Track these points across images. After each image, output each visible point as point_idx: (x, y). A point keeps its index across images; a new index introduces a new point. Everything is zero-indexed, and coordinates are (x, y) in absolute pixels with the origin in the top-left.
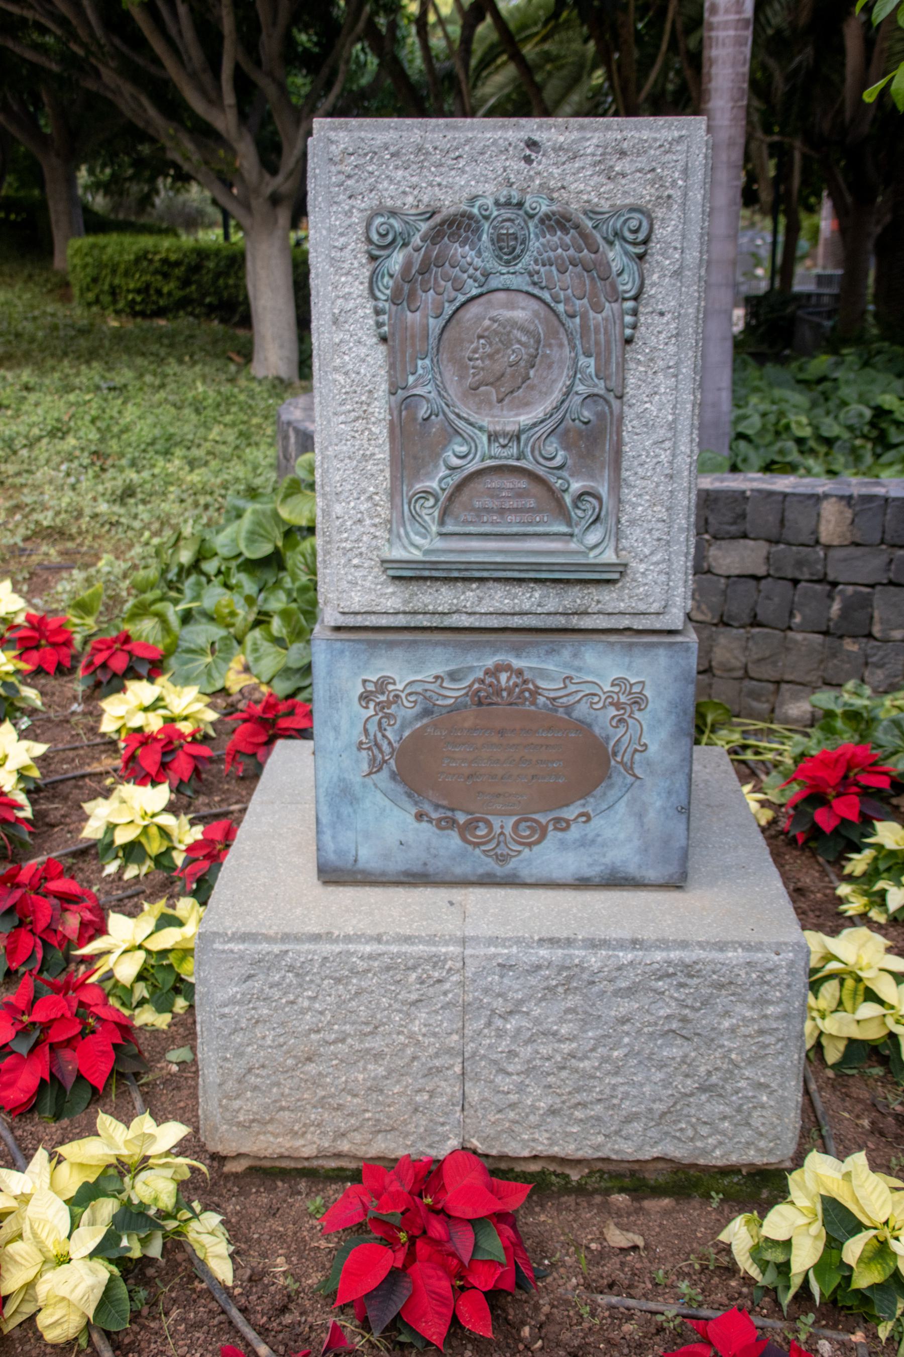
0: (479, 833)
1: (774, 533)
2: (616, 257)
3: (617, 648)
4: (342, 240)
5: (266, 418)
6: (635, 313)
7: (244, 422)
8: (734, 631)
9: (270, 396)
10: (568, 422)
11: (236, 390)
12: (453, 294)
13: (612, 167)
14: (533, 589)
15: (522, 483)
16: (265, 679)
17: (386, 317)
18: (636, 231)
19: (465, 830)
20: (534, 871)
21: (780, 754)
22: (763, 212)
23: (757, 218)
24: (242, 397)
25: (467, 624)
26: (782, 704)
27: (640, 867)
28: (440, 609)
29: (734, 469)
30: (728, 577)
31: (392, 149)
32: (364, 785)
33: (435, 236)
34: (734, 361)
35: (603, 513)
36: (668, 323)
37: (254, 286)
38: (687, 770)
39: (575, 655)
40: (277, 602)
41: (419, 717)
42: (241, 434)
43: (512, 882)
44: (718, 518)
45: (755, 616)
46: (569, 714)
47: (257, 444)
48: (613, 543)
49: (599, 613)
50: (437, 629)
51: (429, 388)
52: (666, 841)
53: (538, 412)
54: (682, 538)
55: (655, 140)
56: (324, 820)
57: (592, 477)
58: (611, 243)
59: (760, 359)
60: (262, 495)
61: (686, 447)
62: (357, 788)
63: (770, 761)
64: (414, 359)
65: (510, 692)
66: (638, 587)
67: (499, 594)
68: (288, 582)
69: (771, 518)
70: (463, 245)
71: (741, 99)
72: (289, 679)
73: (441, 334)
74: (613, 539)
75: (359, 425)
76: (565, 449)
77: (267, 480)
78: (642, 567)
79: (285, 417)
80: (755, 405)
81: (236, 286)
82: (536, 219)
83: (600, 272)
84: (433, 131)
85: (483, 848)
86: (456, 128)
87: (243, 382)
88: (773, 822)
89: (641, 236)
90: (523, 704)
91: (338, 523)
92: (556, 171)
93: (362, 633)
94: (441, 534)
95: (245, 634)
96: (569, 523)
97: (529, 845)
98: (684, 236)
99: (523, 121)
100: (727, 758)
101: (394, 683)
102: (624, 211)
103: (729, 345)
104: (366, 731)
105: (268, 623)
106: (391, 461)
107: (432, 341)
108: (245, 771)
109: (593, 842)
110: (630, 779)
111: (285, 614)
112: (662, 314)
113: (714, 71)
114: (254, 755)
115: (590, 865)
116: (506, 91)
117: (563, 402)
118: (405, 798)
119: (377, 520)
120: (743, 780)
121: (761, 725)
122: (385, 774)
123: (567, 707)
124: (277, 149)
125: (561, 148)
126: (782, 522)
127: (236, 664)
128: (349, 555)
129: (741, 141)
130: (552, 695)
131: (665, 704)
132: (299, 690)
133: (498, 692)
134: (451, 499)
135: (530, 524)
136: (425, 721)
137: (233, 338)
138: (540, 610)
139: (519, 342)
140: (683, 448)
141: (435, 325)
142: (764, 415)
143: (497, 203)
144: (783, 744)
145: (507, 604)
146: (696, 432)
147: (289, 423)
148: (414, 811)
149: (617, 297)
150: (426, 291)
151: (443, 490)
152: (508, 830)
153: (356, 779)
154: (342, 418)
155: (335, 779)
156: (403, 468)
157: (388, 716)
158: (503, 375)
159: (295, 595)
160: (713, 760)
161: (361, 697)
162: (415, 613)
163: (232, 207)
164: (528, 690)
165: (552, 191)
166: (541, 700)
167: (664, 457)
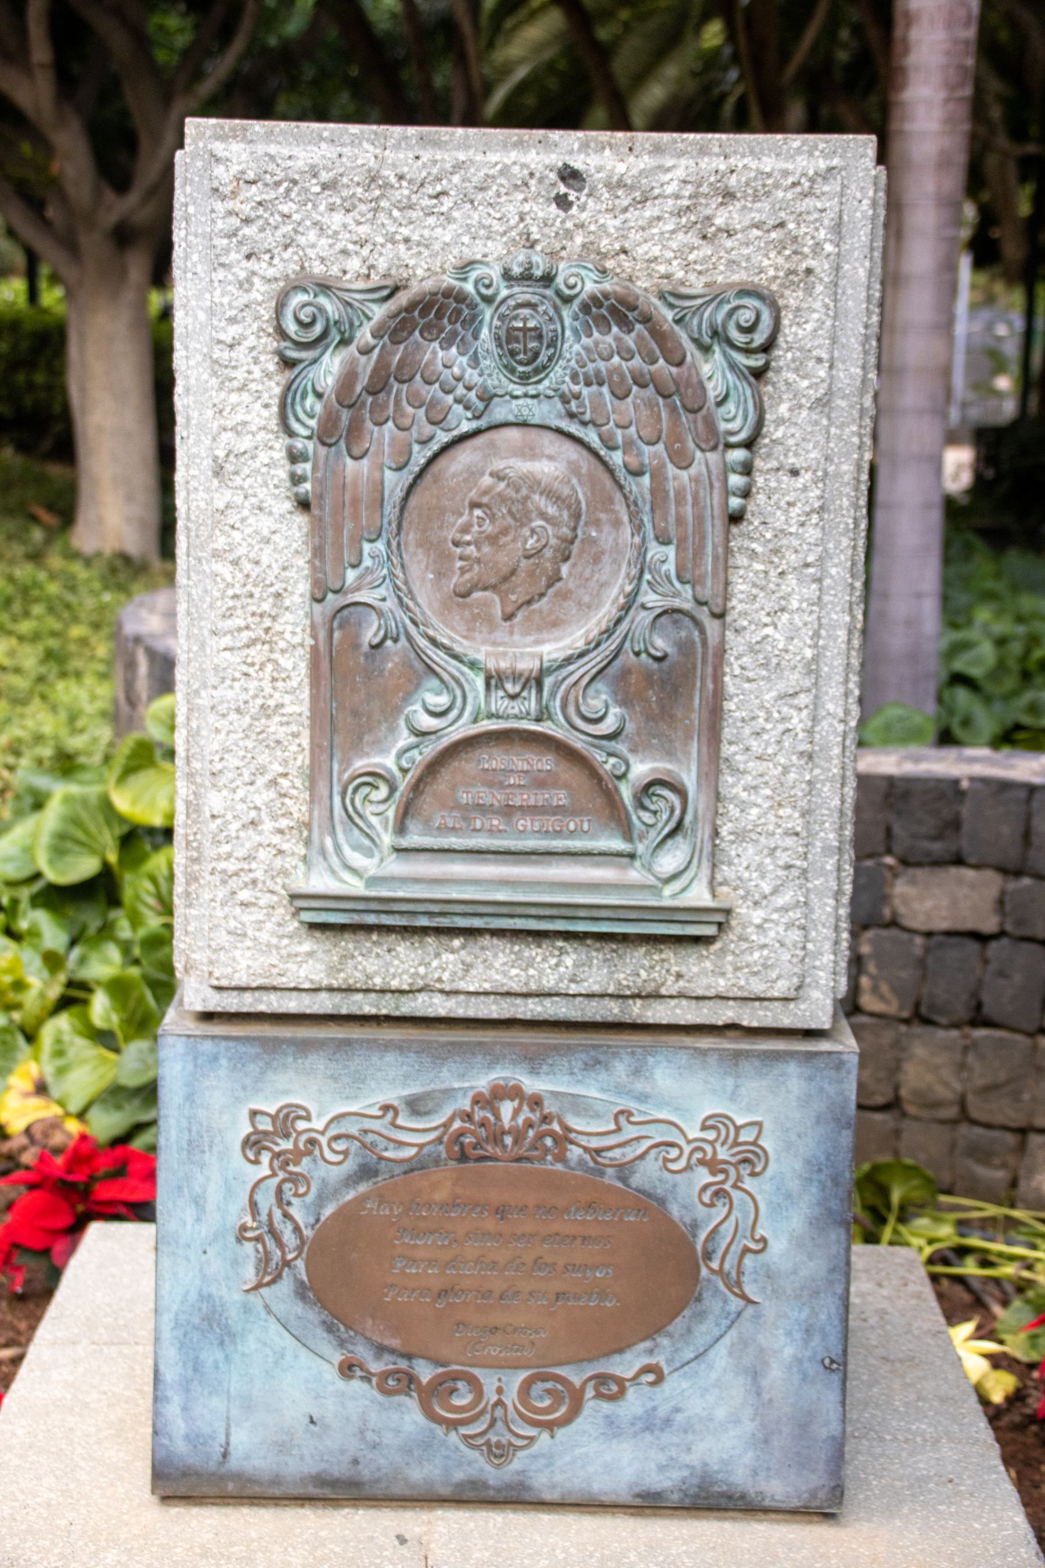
0: (457, 1401)
1: (1012, 855)
2: (714, 372)
3: (713, 1060)
4: (234, 330)
5: (96, 626)
6: (747, 469)
7: (54, 634)
8: (941, 1034)
9: (106, 588)
10: (628, 658)
11: (42, 576)
12: (428, 429)
13: (708, 218)
14: (562, 951)
15: (546, 763)
16: (74, 1107)
17: (308, 466)
18: (750, 330)
19: (431, 1396)
20: (558, 1478)
21: (1030, 1267)
22: (1010, 280)
23: (999, 287)
24: (53, 589)
25: (442, 1012)
26: (1031, 1172)
27: (755, 1473)
28: (395, 984)
29: (946, 738)
30: (929, 934)
31: (325, 176)
32: (247, 1309)
33: (398, 329)
34: (947, 544)
35: (688, 818)
36: (805, 489)
37: (83, 390)
38: (839, 1289)
39: (637, 1072)
40: (104, 965)
41: (352, 1180)
42: (49, 655)
43: (516, 1498)
44: (896, 828)
45: (979, 1006)
46: (624, 1180)
47: (78, 675)
48: (705, 872)
49: (681, 996)
50: (389, 1019)
51: (382, 591)
52: (803, 1425)
53: (574, 638)
54: (830, 864)
55: (786, 173)
56: (169, 1375)
57: (670, 754)
58: (706, 349)
59: (998, 539)
60: (82, 768)
61: (838, 702)
62: (233, 1314)
63: (1009, 1279)
64: (357, 541)
65: (519, 1137)
66: (751, 950)
67: (502, 958)
68: (124, 930)
69: (1005, 830)
70: (446, 344)
71: (962, 85)
72: (119, 1107)
73: (406, 498)
74: (706, 865)
75: (257, 653)
76: (623, 703)
77: (95, 740)
78: (757, 916)
79: (130, 628)
80: (985, 625)
81: (50, 388)
82: (576, 305)
83: (686, 399)
84: (397, 147)
85: (464, 1431)
86: (437, 144)
87: (55, 561)
88: (1017, 1398)
89: (759, 338)
90: (542, 1159)
91: (213, 826)
92: (612, 223)
93: (250, 1025)
94: (398, 850)
95: (40, 1022)
96: (628, 834)
97: (550, 1426)
98: (834, 340)
99: (555, 135)
100: (922, 1272)
101: (308, 1118)
102: (730, 293)
103: (935, 517)
104: (253, 1205)
105: (85, 1003)
106: (313, 718)
107: (390, 510)
108: (28, 1282)
109: (667, 1422)
110: (735, 1304)
111: (118, 988)
112: (795, 473)
113: (914, 34)
114: (45, 1252)
115: (662, 1468)
116: (548, 54)
117: (619, 621)
118: (321, 1332)
119: (284, 823)
120: (953, 1316)
121: (992, 1210)
122: (285, 1287)
123: (621, 1166)
124: (130, 142)
125: (621, 184)
126: (1027, 837)
127: (21, 1079)
128: (233, 883)
129: (961, 159)
130: (595, 1143)
131: (798, 1165)
132: (139, 1128)
133: (497, 1137)
134: (417, 788)
135: (558, 834)
136: (363, 1188)
137: (41, 480)
138: (573, 989)
139: (543, 515)
140: (831, 707)
141: (394, 482)
142: (1001, 642)
143: (507, 275)
144: (1034, 1247)
145: (515, 978)
146: (854, 678)
147: (138, 640)
148: (337, 1357)
149: (715, 441)
150: (380, 424)
151: (404, 771)
152: (511, 1397)
153: (232, 1296)
154: (226, 641)
155: (193, 1296)
156: (333, 731)
157: (294, 1179)
158: (513, 572)
159: (137, 951)
160: (893, 1276)
161: (247, 1143)
162: (350, 990)
163: (42, 244)
164: (552, 1134)
165: (605, 256)
166: (574, 1153)
167: (798, 721)
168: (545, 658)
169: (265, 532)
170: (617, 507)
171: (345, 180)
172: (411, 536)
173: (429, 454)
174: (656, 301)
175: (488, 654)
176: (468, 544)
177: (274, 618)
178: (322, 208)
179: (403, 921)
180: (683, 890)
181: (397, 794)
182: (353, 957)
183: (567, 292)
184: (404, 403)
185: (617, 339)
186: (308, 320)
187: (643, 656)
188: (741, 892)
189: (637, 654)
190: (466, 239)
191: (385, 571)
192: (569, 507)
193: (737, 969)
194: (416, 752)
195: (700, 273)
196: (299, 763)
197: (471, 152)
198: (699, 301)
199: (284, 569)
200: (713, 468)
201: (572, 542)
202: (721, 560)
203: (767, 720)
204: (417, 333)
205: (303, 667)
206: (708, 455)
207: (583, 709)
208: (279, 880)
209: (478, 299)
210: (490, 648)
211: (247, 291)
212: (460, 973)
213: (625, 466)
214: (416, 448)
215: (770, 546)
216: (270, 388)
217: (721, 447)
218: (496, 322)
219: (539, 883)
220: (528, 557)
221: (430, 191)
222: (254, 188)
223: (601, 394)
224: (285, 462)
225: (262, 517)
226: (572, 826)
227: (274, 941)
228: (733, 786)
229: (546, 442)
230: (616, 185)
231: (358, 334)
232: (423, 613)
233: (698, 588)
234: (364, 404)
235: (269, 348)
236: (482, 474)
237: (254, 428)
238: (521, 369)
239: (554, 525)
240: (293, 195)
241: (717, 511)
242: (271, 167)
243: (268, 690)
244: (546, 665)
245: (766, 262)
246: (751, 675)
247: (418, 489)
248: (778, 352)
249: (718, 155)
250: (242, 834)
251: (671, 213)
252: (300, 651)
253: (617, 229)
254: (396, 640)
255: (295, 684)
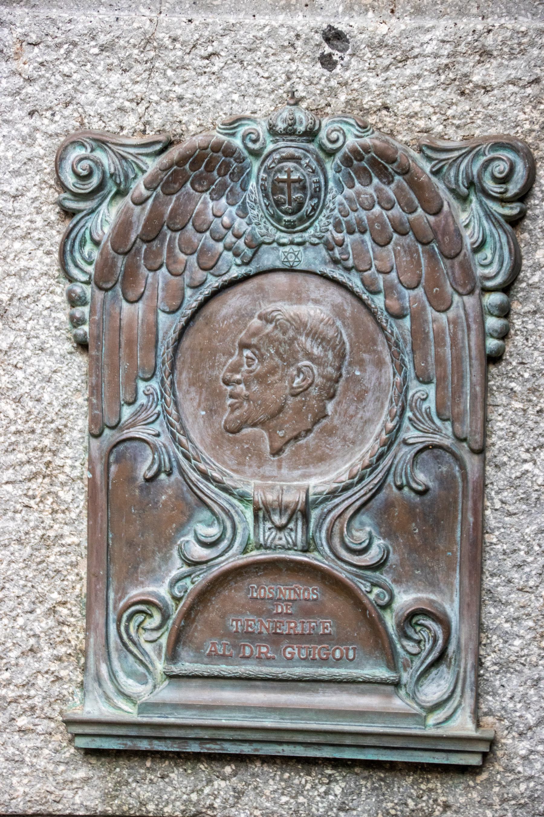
2: (471, 220)
4: (17, 183)
6: (505, 312)
10: (390, 491)
12: (200, 275)
13: (466, 75)
14: (331, 779)
15: (312, 592)
17: (86, 310)
18: (505, 180)
31: (103, 39)
33: (171, 181)
35: (452, 648)
48: (469, 701)
51: (157, 427)
53: (339, 472)
58: (464, 199)
64: (132, 380)
67: (272, 785)
70: (217, 195)
74: (469, 696)
75: (37, 487)
76: (385, 535)
83: (443, 244)
89: (513, 188)
92: (374, 81)
94: (171, 677)
96: (392, 662)
107: (164, 351)
117: (381, 456)
119: (62, 650)
125: (382, 44)
128: (12, 710)
134: (189, 615)
135: (324, 662)
139: (309, 356)
141: (168, 324)
143: (272, 130)
149: (472, 286)
151: (177, 599)
156: (109, 561)
158: (281, 409)
165: (368, 112)
168: (311, 492)
169: (47, 371)
170: (380, 348)
171: (122, 42)
172: (184, 375)
173: (201, 298)
174: (416, 155)
175: (256, 487)
176: (238, 382)
177: (54, 453)
178: (100, 68)
179: (175, 748)
180: (447, 719)
181: (170, 622)
182: (127, 783)
183: (330, 146)
184: (177, 250)
185: (378, 190)
186: (85, 173)
187: (406, 489)
188: (506, 723)
189: (400, 488)
190: (236, 97)
191: (159, 408)
192: (333, 348)
193: (504, 801)
194: (188, 581)
195: (458, 127)
196: (77, 591)
197: (241, 16)
198: (456, 154)
199: (65, 406)
200: (470, 311)
201: (337, 381)
202: (480, 399)
203: (527, 553)
204: (188, 185)
205: (82, 498)
206: (465, 298)
207: (347, 540)
208: (56, 707)
209: (246, 153)
210: (259, 482)
211: (30, 146)
212: (231, 801)
213: (387, 309)
214: (188, 292)
215: (529, 385)
216: (52, 237)
217: (477, 291)
218: (263, 175)
219: (305, 710)
220: (295, 395)
221: (203, 53)
222: (36, 49)
223: (363, 241)
224: (66, 305)
225: (43, 357)
226: (338, 654)
227: (51, 767)
228: (496, 617)
229: (312, 287)
230: (378, 45)
231: (133, 186)
232: (195, 448)
233: (457, 425)
234: (139, 251)
235: (51, 199)
236: (252, 317)
237: (36, 274)
238: (287, 218)
239: (319, 364)
240: (73, 56)
241: (474, 353)
242: (52, 30)
243: (48, 522)
244: (311, 498)
245: (522, 116)
246: (511, 509)
247: (191, 331)
248: (534, 202)
249: (476, 16)
250: (21, 661)
251: (431, 72)
252: (79, 484)
253: (379, 86)
254: (169, 474)
255: (73, 515)
